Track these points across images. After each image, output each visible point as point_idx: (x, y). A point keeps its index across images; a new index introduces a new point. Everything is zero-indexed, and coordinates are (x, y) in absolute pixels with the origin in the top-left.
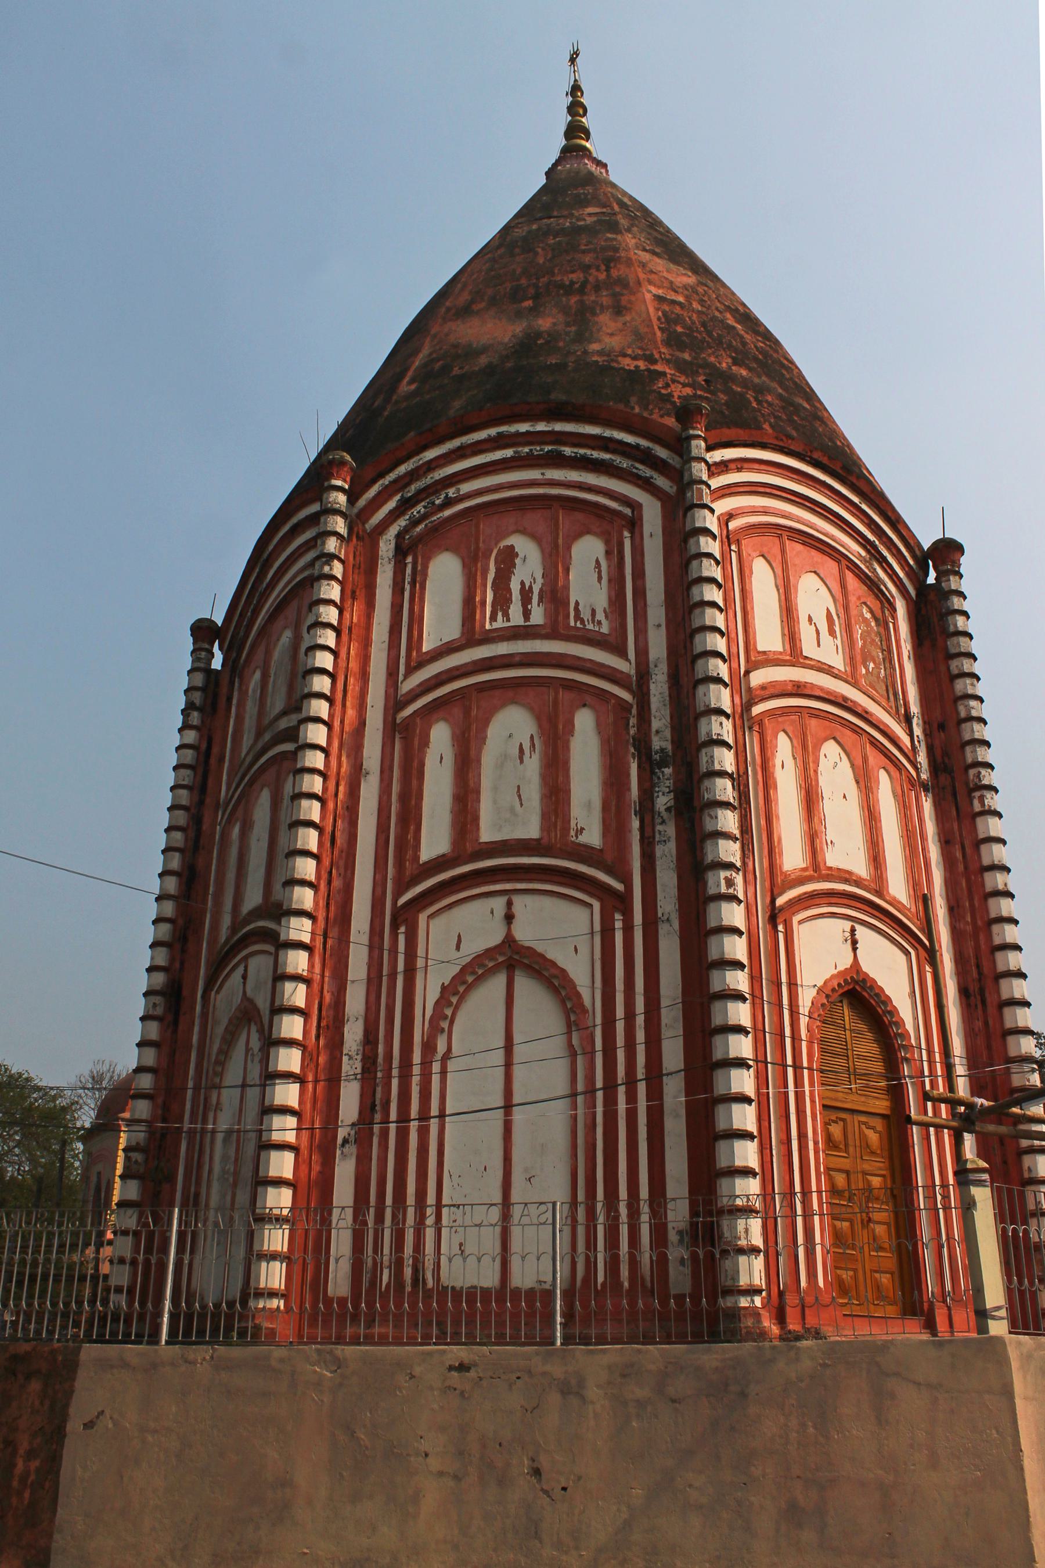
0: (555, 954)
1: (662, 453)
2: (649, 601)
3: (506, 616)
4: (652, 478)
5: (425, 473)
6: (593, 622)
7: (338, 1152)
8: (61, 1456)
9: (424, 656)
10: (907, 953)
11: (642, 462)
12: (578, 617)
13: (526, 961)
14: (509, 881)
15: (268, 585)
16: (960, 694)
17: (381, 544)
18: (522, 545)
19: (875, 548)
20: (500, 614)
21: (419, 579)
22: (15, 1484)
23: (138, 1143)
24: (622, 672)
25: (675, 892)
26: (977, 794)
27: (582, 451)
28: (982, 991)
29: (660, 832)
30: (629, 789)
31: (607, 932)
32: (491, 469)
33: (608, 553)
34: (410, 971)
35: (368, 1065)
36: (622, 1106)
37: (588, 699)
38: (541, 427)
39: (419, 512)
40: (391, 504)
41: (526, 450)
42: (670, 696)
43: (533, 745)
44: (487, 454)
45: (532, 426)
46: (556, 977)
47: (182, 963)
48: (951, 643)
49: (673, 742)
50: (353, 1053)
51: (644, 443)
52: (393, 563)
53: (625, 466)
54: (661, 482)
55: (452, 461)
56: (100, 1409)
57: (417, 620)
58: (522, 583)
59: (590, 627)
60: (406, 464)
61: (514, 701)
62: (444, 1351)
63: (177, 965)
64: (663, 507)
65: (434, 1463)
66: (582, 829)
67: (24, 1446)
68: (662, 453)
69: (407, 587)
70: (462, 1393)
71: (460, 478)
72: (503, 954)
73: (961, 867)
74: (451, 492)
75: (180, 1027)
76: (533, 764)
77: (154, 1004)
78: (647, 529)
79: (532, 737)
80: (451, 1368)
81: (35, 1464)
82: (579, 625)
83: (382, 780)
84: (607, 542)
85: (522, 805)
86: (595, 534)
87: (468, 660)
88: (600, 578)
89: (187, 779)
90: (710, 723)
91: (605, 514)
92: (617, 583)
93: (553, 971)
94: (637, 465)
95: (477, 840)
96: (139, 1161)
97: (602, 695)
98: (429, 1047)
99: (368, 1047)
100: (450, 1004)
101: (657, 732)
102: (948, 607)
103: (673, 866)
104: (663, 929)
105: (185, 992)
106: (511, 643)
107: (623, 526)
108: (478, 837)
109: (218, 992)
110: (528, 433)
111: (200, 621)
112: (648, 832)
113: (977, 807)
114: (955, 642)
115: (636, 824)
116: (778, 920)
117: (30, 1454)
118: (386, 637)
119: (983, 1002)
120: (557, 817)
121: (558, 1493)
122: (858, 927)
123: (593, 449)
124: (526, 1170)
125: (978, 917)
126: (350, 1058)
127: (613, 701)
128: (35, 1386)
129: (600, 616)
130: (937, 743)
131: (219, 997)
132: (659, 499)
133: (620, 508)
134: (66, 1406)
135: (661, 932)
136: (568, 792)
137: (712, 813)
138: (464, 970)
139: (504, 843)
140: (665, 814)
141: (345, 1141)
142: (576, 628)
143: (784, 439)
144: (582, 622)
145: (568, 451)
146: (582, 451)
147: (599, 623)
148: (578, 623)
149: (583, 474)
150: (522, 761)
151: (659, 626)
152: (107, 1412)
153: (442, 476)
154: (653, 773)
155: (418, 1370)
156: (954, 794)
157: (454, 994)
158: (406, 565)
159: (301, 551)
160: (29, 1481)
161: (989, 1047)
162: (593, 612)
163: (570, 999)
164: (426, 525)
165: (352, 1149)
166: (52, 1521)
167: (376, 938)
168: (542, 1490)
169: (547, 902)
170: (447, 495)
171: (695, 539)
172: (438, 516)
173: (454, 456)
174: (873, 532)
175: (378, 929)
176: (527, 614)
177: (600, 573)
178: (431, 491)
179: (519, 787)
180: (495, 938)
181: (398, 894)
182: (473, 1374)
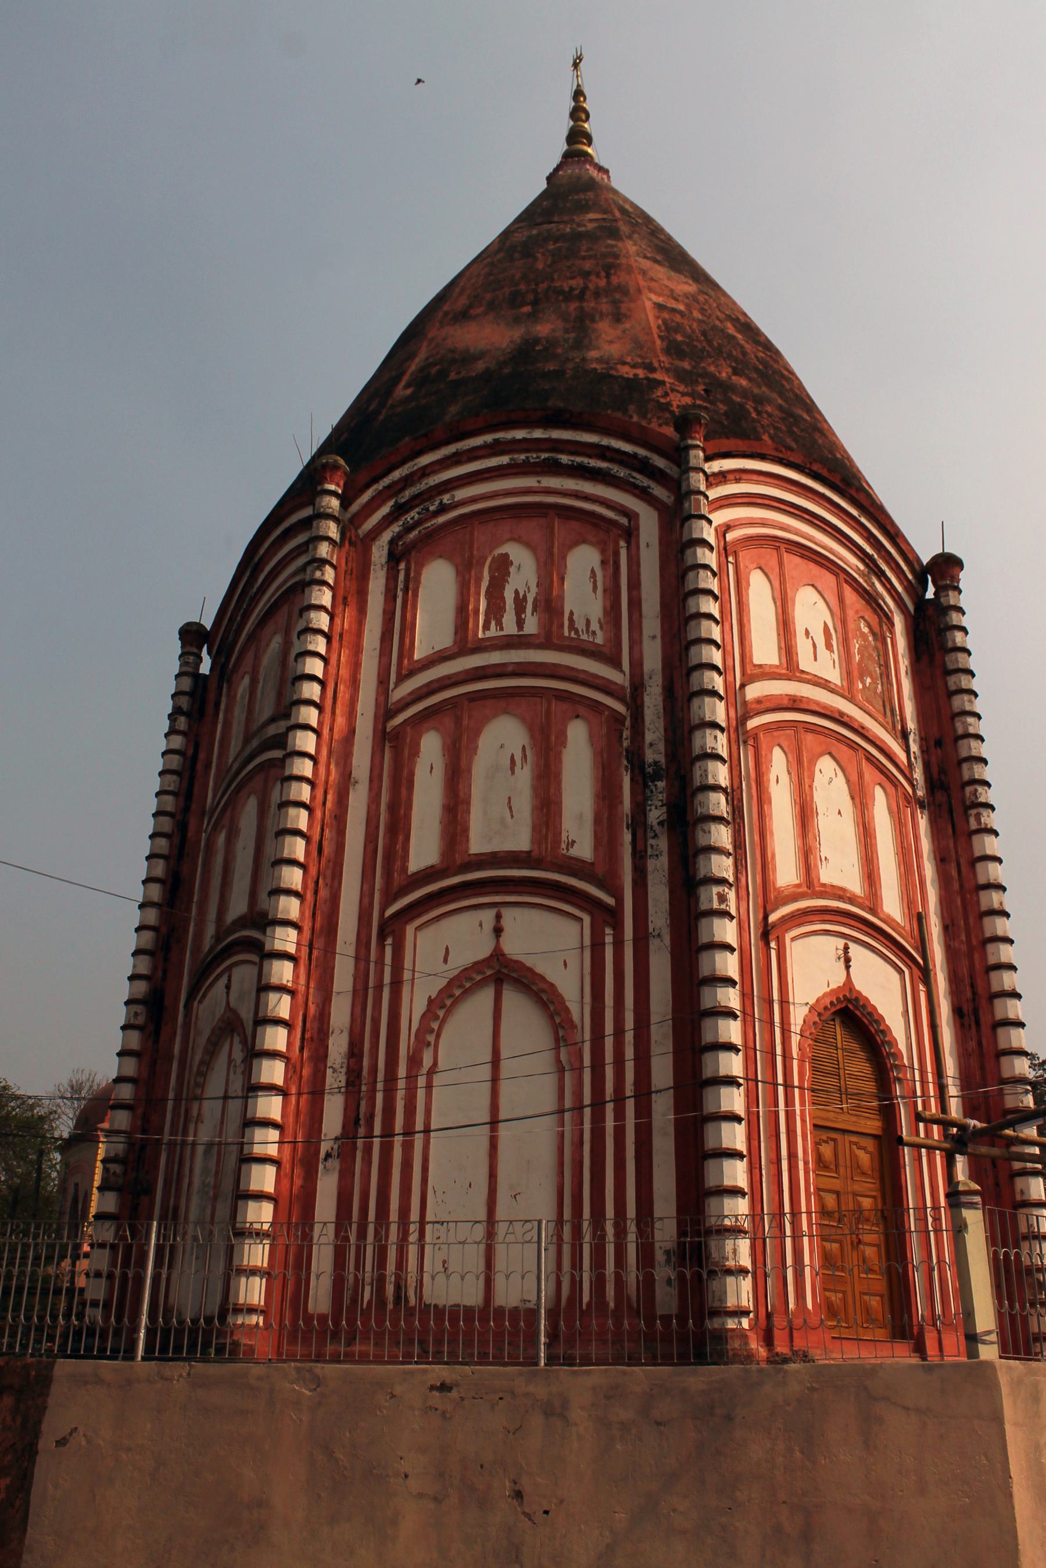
1: (660, 462)
3: (500, 625)
7: (321, 1167)
10: (901, 972)
13: (514, 975)
14: (497, 893)
15: (259, 589)
18: (517, 553)
20: (493, 623)
21: (412, 586)
26: (973, 812)
27: (579, 459)
28: (976, 1012)
29: (652, 846)
30: (622, 803)
31: (597, 947)
33: (603, 563)
34: (397, 984)
38: (538, 434)
39: (412, 518)
40: (385, 510)
41: (523, 457)
43: (525, 756)
45: (529, 433)
46: (543, 991)
47: (165, 971)
49: (666, 756)
50: (337, 1066)
51: (642, 452)
52: (385, 569)
53: (622, 475)
55: (447, 467)
56: (73, 1426)
57: (407, 627)
58: (517, 592)
59: (584, 637)
63: (160, 974)
65: (414, 1485)
66: (574, 842)
68: (660, 462)
69: (400, 594)
70: (444, 1413)
71: (455, 484)
73: (956, 886)
74: (446, 499)
76: (524, 776)
78: (643, 538)
79: (524, 747)
80: (432, 1388)
82: (573, 635)
84: (603, 552)
85: (512, 816)
86: (591, 544)
89: (173, 785)
92: (612, 593)
93: (544, 986)
94: (635, 474)
95: (467, 852)
97: (596, 707)
101: (651, 745)
102: (947, 623)
103: (665, 880)
104: (654, 945)
107: (620, 536)
108: (468, 848)
110: (524, 440)
111: (188, 624)
113: (973, 825)
115: (627, 837)
116: (771, 937)
118: (377, 644)
119: (978, 1023)
121: (539, 1516)
122: (851, 945)
123: (590, 457)
125: (973, 937)
126: (335, 1071)
129: (595, 626)
130: (933, 759)
132: (656, 508)
133: (617, 518)
135: (652, 947)
138: (451, 983)
139: (494, 854)
141: (328, 1155)
142: (570, 638)
144: (577, 631)
145: (565, 459)
146: (579, 459)
147: (594, 633)
150: (513, 773)
151: (654, 637)
153: (437, 482)
154: (646, 786)
155: (398, 1390)
156: (951, 812)
157: (441, 1008)
158: (398, 571)
159: (293, 555)
161: (982, 1068)
162: (588, 623)
163: (558, 1014)
165: (335, 1164)
167: (363, 950)
168: (524, 1513)
171: (692, 549)
172: (432, 523)
176: (520, 624)
178: (425, 497)
179: (510, 798)
180: (484, 952)
182: (454, 1394)
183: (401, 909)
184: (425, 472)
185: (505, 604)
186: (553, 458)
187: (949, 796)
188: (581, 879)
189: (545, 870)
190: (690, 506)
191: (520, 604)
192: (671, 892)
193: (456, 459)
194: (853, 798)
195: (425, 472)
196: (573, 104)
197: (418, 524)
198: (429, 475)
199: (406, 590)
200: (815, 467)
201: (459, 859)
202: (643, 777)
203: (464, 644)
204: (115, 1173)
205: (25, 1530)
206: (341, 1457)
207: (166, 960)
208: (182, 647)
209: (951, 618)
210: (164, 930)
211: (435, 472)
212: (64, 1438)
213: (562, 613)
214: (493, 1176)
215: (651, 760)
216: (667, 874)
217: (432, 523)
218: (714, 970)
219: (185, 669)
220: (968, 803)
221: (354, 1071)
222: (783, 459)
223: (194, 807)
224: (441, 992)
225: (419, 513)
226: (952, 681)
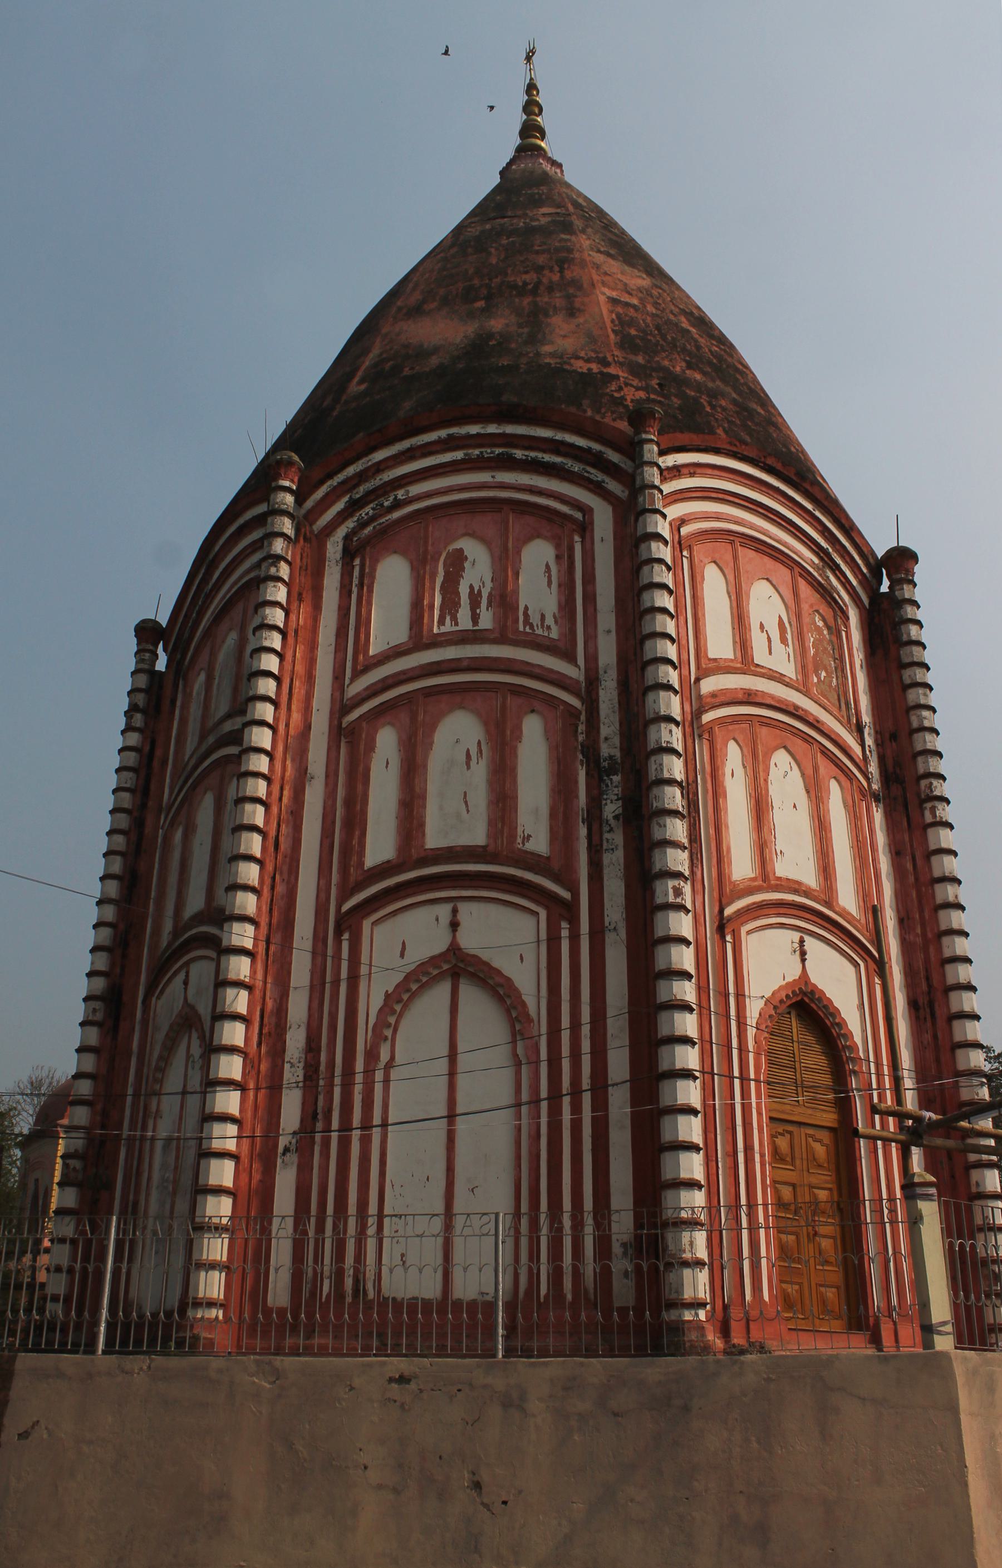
0: (498, 962)
1: (614, 456)
3: (455, 620)
4: (603, 482)
5: (374, 474)
7: (279, 1161)
10: (856, 965)
11: (594, 466)
14: (454, 888)
17: (329, 546)
18: (475, 551)
20: (448, 619)
24: (571, 678)
26: (929, 805)
27: (533, 454)
28: (931, 1004)
29: (608, 840)
30: (577, 797)
31: (553, 941)
32: (441, 471)
33: (558, 557)
36: (567, 1116)
38: (492, 429)
39: (367, 514)
41: (477, 452)
43: (480, 751)
45: (483, 428)
46: (502, 986)
48: (904, 652)
49: (621, 749)
50: (295, 1061)
51: (596, 447)
53: (576, 469)
56: (35, 1419)
57: (364, 623)
58: (471, 587)
61: (461, 707)
62: (384, 1363)
63: (118, 970)
66: (529, 836)
68: (614, 456)
69: (355, 590)
70: (402, 1405)
73: (912, 879)
74: (400, 494)
76: (480, 771)
79: (479, 743)
80: (391, 1380)
82: (528, 629)
84: (557, 547)
85: (468, 811)
88: (550, 583)
90: (659, 731)
93: (498, 979)
94: (589, 469)
95: (423, 846)
97: (551, 701)
100: (393, 1012)
101: (606, 739)
103: (620, 874)
104: (610, 938)
106: (459, 647)
110: (478, 435)
111: (144, 621)
113: (928, 818)
118: (332, 640)
122: (806, 938)
123: (544, 451)
125: (928, 929)
126: (292, 1065)
127: (562, 707)
129: (550, 621)
132: (610, 503)
140: (612, 822)
141: (286, 1150)
143: (738, 444)
144: (532, 627)
145: (519, 454)
146: (533, 454)
147: (549, 628)
151: (609, 632)
153: (391, 477)
155: (357, 1382)
156: (906, 806)
158: (353, 567)
161: (938, 1060)
163: (515, 1008)
164: (374, 527)
165: (293, 1158)
168: (483, 1504)
169: (493, 909)
170: (396, 497)
171: (647, 543)
172: (387, 518)
174: (826, 539)
176: (475, 618)
177: (550, 578)
179: (465, 793)
180: (440, 946)
181: (342, 900)
182: (413, 1386)
184: (379, 467)
185: (460, 599)
192: (627, 887)
193: (410, 455)
195: (379, 467)
197: (372, 519)
199: (361, 585)
200: (770, 461)
201: (415, 854)
206: (301, 1448)
208: (138, 644)
211: (389, 468)
213: (518, 608)
214: (450, 1169)
215: (606, 755)
217: (387, 518)
218: (671, 963)
223: (150, 803)
224: (397, 986)
225: (373, 509)
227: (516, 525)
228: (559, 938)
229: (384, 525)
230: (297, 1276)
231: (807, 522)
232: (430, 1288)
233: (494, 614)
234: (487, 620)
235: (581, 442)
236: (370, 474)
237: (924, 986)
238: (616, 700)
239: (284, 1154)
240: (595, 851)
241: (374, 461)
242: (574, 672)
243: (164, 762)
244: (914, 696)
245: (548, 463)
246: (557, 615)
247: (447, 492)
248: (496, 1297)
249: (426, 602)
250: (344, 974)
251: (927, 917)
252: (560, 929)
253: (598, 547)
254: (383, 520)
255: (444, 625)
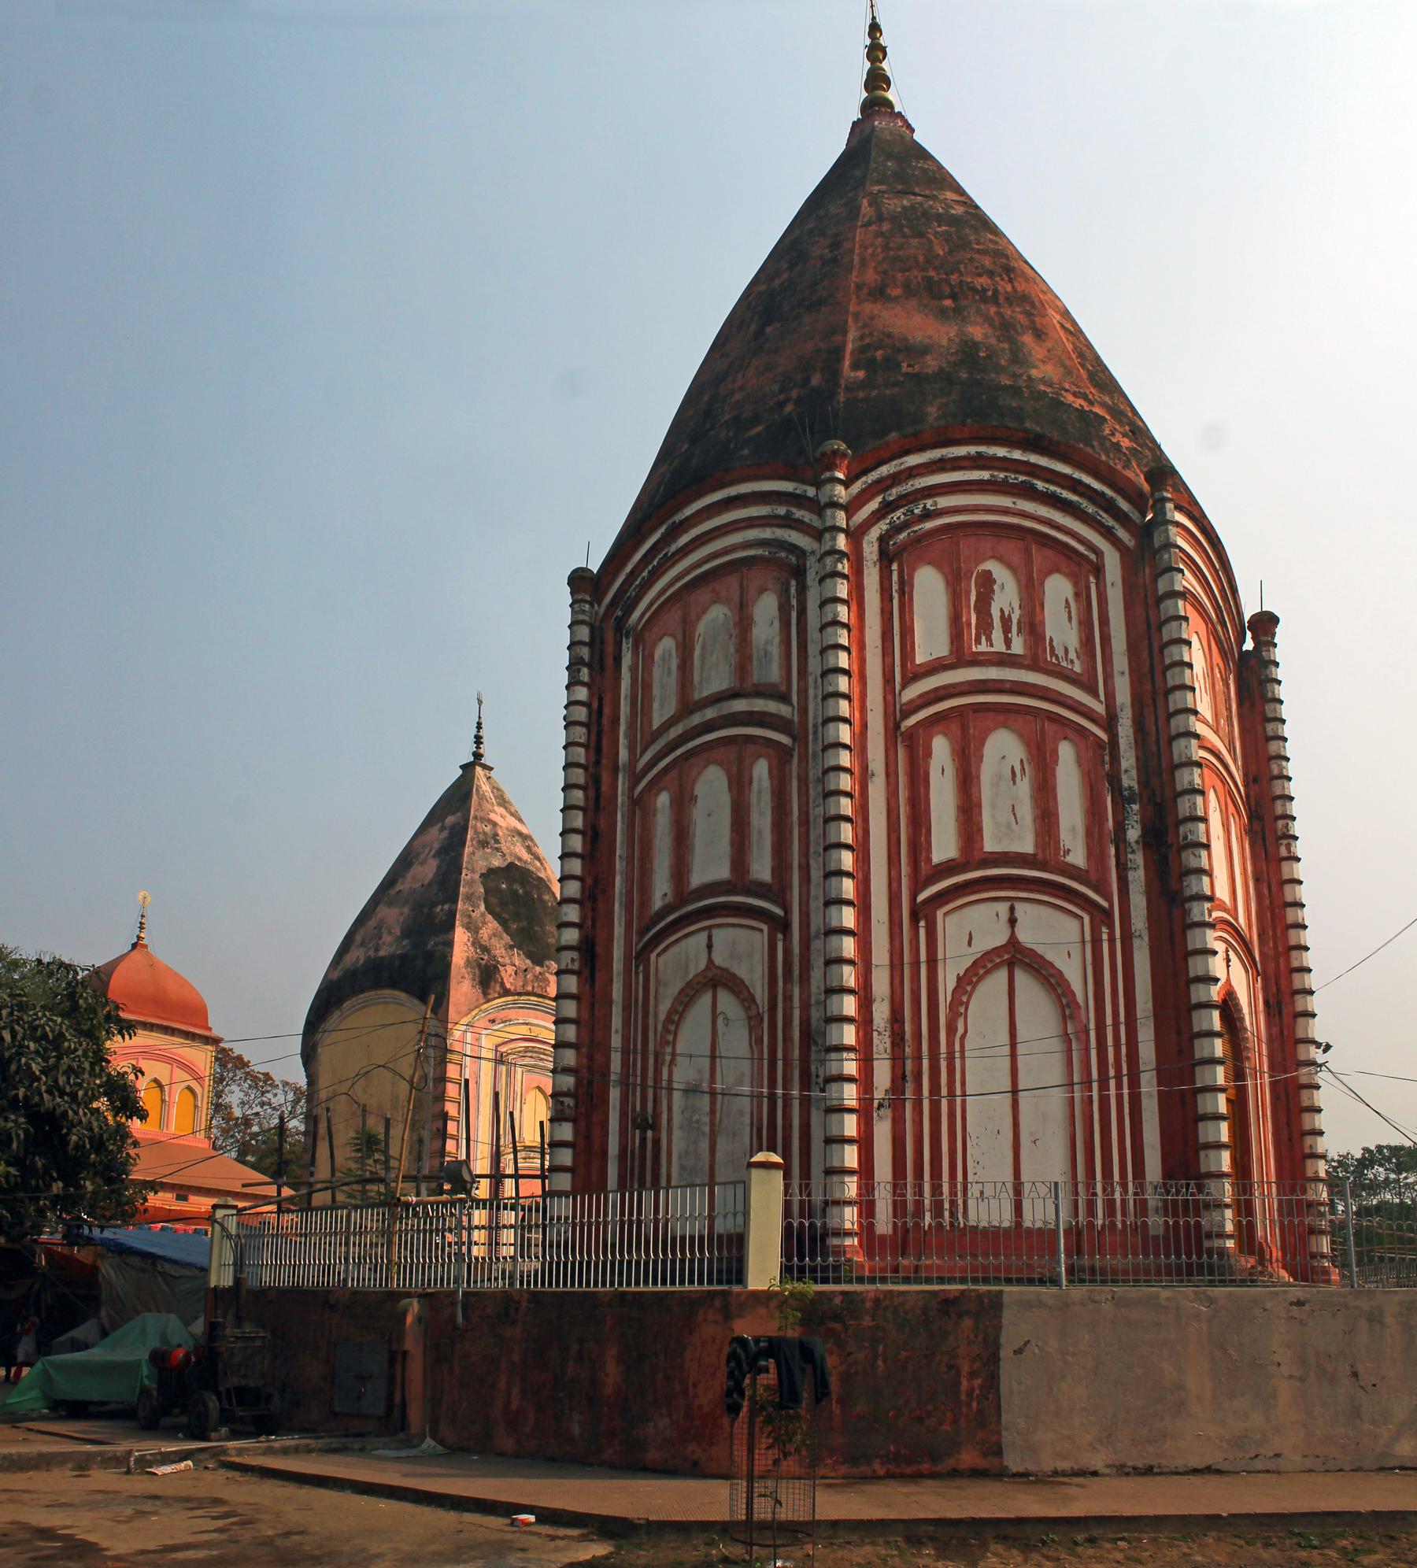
1: (1124, 505)
2: (1113, 650)
3: (989, 640)
4: (1113, 528)
6: (1067, 660)
7: (875, 1115)
8: (999, 1376)
9: (918, 668)
10: (1247, 971)
11: (1106, 511)
12: (1053, 653)
13: (1027, 960)
14: (1013, 889)
15: (679, 551)
16: (1273, 754)
17: (865, 545)
19: (1221, 612)
20: (983, 638)
22: (963, 1397)
23: (569, 1089)
24: (1097, 712)
25: (1145, 912)
26: (1285, 842)
27: (1053, 488)
28: (1279, 1004)
29: (1131, 860)
30: (1107, 820)
31: (1096, 942)
32: (967, 488)
33: (1077, 595)
35: (897, 1041)
36: (1113, 1092)
37: (1071, 734)
38: (1017, 455)
39: (899, 518)
40: (874, 505)
41: (1002, 475)
42: (1135, 740)
43: (1023, 769)
44: (966, 472)
45: (1008, 452)
46: (1052, 976)
47: (593, 920)
48: (1269, 707)
49: (1139, 782)
51: (1109, 492)
52: (878, 566)
53: (1090, 511)
54: (1121, 533)
55: (933, 472)
56: (1026, 1339)
57: (907, 632)
58: (1002, 610)
59: (1064, 664)
60: (888, 465)
61: (1005, 726)
62: (1286, 1292)
63: (589, 922)
64: (1122, 557)
65: (1285, 1370)
66: (1069, 850)
67: (965, 1369)
68: (1124, 505)
69: (895, 595)
70: (1301, 1321)
71: (938, 491)
72: (1009, 953)
73: (1267, 902)
74: (929, 503)
75: (597, 983)
76: (1024, 788)
77: (572, 959)
78: (1109, 578)
79: (1022, 760)
80: (1292, 1304)
81: (977, 1382)
82: (1054, 660)
83: (888, 783)
84: (1076, 584)
85: (1017, 823)
87: (961, 680)
89: (583, 737)
90: (1192, 774)
91: (1073, 556)
92: (1086, 625)
93: (1052, 971)
94: (1101, 513)
95: (982, 849)
96: (571, 1105)
97: (1082, 731)
98: (951, 1029)
99: (896, 1026)
100: (966, 992)
101: (1126, 771)
102: (1267, 675)
103: (1142, 889)
104: (1136, 943)
105: (599, 950)
106: (1000, 668)
107: (1090, 571)
108: (982, 847)
109: (658, 955)
110: (1004, 459)
112: (1122, 861)
113: (1283, 852)
114: (1272, 708)
115: (1113, 851)
116: (920, 915)
117: (972, 1375)
118: (879, 643)
120: (1050, 838)
121: (1370, 1388)
123: (1063, 488)
124: (1032, 1134)
125: (1280, 945)
126: (879, 1034)
127: (1091, 738)
128: (967, 1323)
129: (1072, 655)
130: (1252, 793)
131: (661, 960)
132: (1118, 549)
133: (1086, 553)
134: (997, 1337)
136: (1057, 816)
137: (1196, 853)
138: (975, 963)
139: (1006, 854)
141: (880, 1106)
142: (1051, 662)
144: (1057, 658)
145: (1040, 485)
146: (1053, 488)
147: (1072, 661)
148: (1054, 658)
149: (1051, 511)
151: (1123, 673)
152: (1033, 1342)
153: (922, 485)
155: (1268, 1305)
156: (1264, 840)
157: (969, 984)
158: (891, 571)
160: (975, 1395)
161: (1283, 1051)
162: (1066, 651)
163: (1065, 996)
164: (909, 534)
165: (887, 1112)
166: (999, 1422)
167: (897, 930)
168: (1360, 1386)
169: (1043, 910)
170: (925, 507)
171: (1173, 601)
172: (920, 527)
173: (934, 468)
174: (1222, 598)
175: (897, 922)
176: (1008, 642)
177: (1070, 613)
178: (911, 498)
179: (1013, 806)
180: (1001, 939)
181: (1096, 695)
182: (1307, 1307)
183: (931, 896)
184: (913, 472)
185: (992, 620)
186: (1029, 482)
187: (1263, 825)
188: (1081, 883)
189: (1051, 873)
190: (1170, 558)
191: (1006, 622)
192: (1149, 901)
193: (940, 466)
194: (1223, 826)
195: (913, 472)
196: (868, 65)
198: (915, 477)
199: (902, 592)
202: (1122, 800)
203: (960, 657)
204: (569, 1105)
205: (1000, 1416)
206: (1233, 1353)
207: (594, 910)
208: (572, 593)
209: (1271, 671)
210: (589, 881)
211: (921, 475)
212: (1019, 1349)
215: (1126, 785)
216: (1143, 885)
217: (920, 527)
218: (1208, 971)
219: (581, 617)
220: (1279, 834)
221: (898, 1034)
222: (1191, 512)
223: (604, 761)
224: (967, 970)
225: (904, 514)
226: (1270, 728)
227: (1040, 557)
228: (1101, 940)
229: (918, 534)
230: (899, 1208)
231: (1214, 581)
232: (1004, 1218)
233: (1025, 641)
234: (1018, 647)
235: (1096, 485)
236: (903, 477)
237: (1274, 990)
238: (1132, 738)
239: (878, 1109)
240: (1122, 868)
241: (907, 465)
242: (1100, 708)
243: (615, 721)
244: (1273, 747)
245: (1066, 499)
246: (1078, 650)
247: (964, 511)
248: (1057, 1225)
249: (964, 620)
250: (923, 957)
251: (1279, 935)
252: (1101, 932)
253: (1110, 591)
254: (916, 528)
255: (980, 644)
